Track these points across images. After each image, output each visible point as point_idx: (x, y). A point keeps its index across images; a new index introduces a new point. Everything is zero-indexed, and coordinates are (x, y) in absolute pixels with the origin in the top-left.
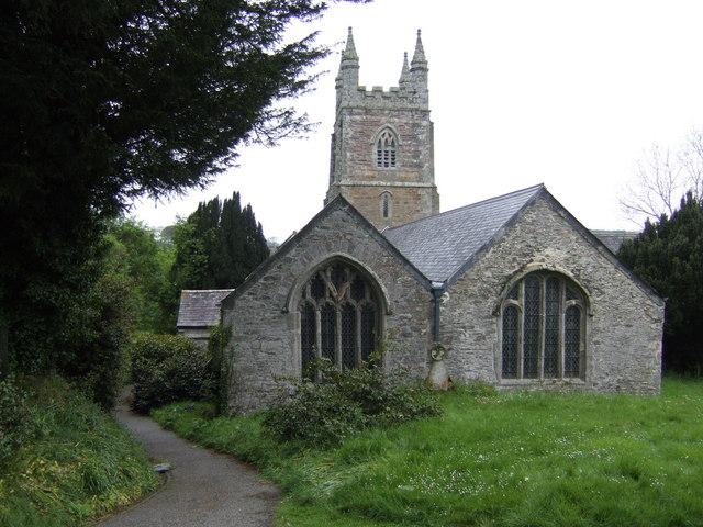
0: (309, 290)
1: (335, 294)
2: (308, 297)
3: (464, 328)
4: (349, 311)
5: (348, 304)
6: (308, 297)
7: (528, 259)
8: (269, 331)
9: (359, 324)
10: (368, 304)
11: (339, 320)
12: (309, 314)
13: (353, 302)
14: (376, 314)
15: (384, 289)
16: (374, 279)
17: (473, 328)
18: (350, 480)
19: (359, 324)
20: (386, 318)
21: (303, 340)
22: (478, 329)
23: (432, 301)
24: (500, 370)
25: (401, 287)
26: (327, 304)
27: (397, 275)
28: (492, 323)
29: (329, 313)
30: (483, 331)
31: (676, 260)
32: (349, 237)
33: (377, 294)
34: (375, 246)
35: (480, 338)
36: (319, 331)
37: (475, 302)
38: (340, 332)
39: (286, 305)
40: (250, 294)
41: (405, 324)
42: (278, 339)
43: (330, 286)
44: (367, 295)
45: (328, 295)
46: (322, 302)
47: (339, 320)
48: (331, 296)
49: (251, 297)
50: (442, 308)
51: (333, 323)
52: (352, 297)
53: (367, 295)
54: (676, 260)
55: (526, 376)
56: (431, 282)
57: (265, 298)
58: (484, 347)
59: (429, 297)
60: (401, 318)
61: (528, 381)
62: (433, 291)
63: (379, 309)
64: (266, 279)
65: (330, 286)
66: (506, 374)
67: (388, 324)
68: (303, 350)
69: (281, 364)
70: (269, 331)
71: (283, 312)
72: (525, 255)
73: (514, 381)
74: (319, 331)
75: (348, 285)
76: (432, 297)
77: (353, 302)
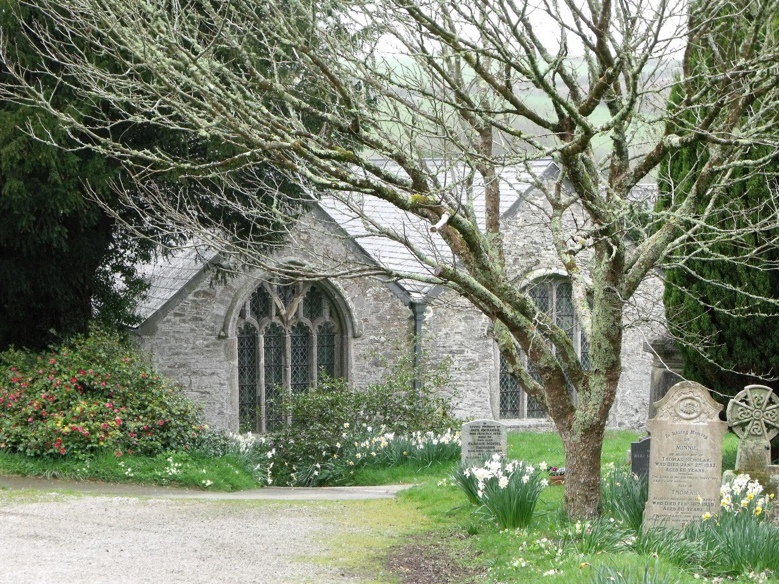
0: (248, 308)
1: (283, 312)
2: (249, 316)
3: (451, 352)
4: (302, 331)
5: (300, 325)
6: (249, 316)
7: (533, 259)
8: (199, 362)
9: (315, 351)
10: (327, 324)
11: (289, 345)
12: (248, 339)
13: (307, 322)
14: (337, 338)
15: (351, 305)
16: (337, 291)
17: (462, 352)
18: (574, 424)
19: (315, 351)
20: (352, 342)
21: (241, 374)
22: (469, 354)
23: (410, 318)
24: (497, 408)
25: (372, 301)
26: (273, 325)
27: (367, 286)
28: (488, 345)
29: (275, 335)
30: (476, 356)
31: (270, 481)
32: (305, 237)
33: (340, 311)
34: (338, 249)
35: (472, 366)
36: (262, 361)
37: (466, 318)
38: (289, 362)
39: (225, 328)
40: (176, 315)
41: (377, 350)
42: (213, 374)
43: (277, 301)
44: (326, 311)
45: (274, 313)
46: (267, 322)
47: (289, 345)
48: (278, 314)
49: (178, 318)
50: (423, 327)
51: (281, 351)
52: (306, 315)
53: (326, 311)
54: (270, 481)
55: (531, 413)
56: (408, 293)
57: (195, 319)
58: (477, 378)
59: (407, 312)
60: (373, 342)
61: (533, 421)
62: (412, 305)
63: (343, 331)
64: (197, 294)
65: (277, 301)
66: (504, 413)
67: (355, 349)
68: (242, 387)
69: (218, 406)
70: (199, 362)
71: (220, 337)
72: (530, 255)
73: (515, 422)
74: (262, 361)
75: (300, 300)
76: (411, 314)
77: (307, 322)
